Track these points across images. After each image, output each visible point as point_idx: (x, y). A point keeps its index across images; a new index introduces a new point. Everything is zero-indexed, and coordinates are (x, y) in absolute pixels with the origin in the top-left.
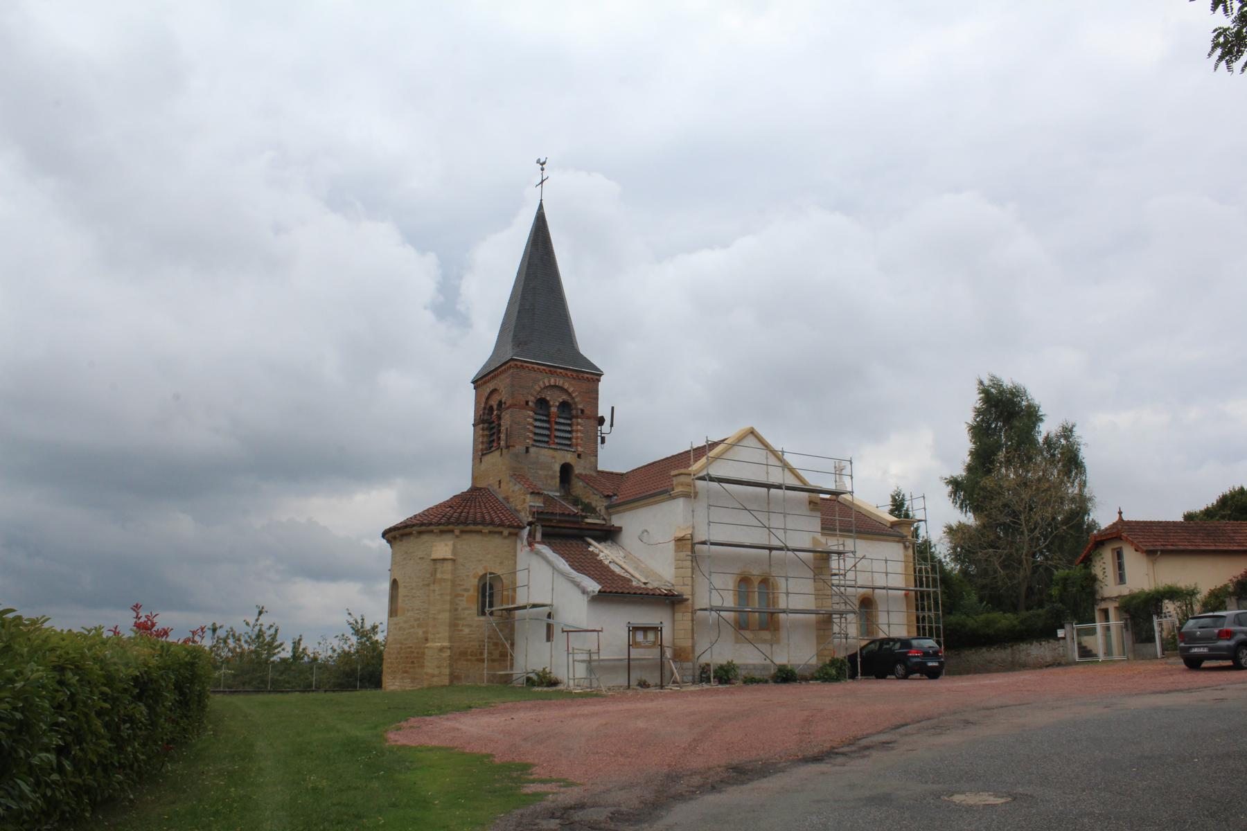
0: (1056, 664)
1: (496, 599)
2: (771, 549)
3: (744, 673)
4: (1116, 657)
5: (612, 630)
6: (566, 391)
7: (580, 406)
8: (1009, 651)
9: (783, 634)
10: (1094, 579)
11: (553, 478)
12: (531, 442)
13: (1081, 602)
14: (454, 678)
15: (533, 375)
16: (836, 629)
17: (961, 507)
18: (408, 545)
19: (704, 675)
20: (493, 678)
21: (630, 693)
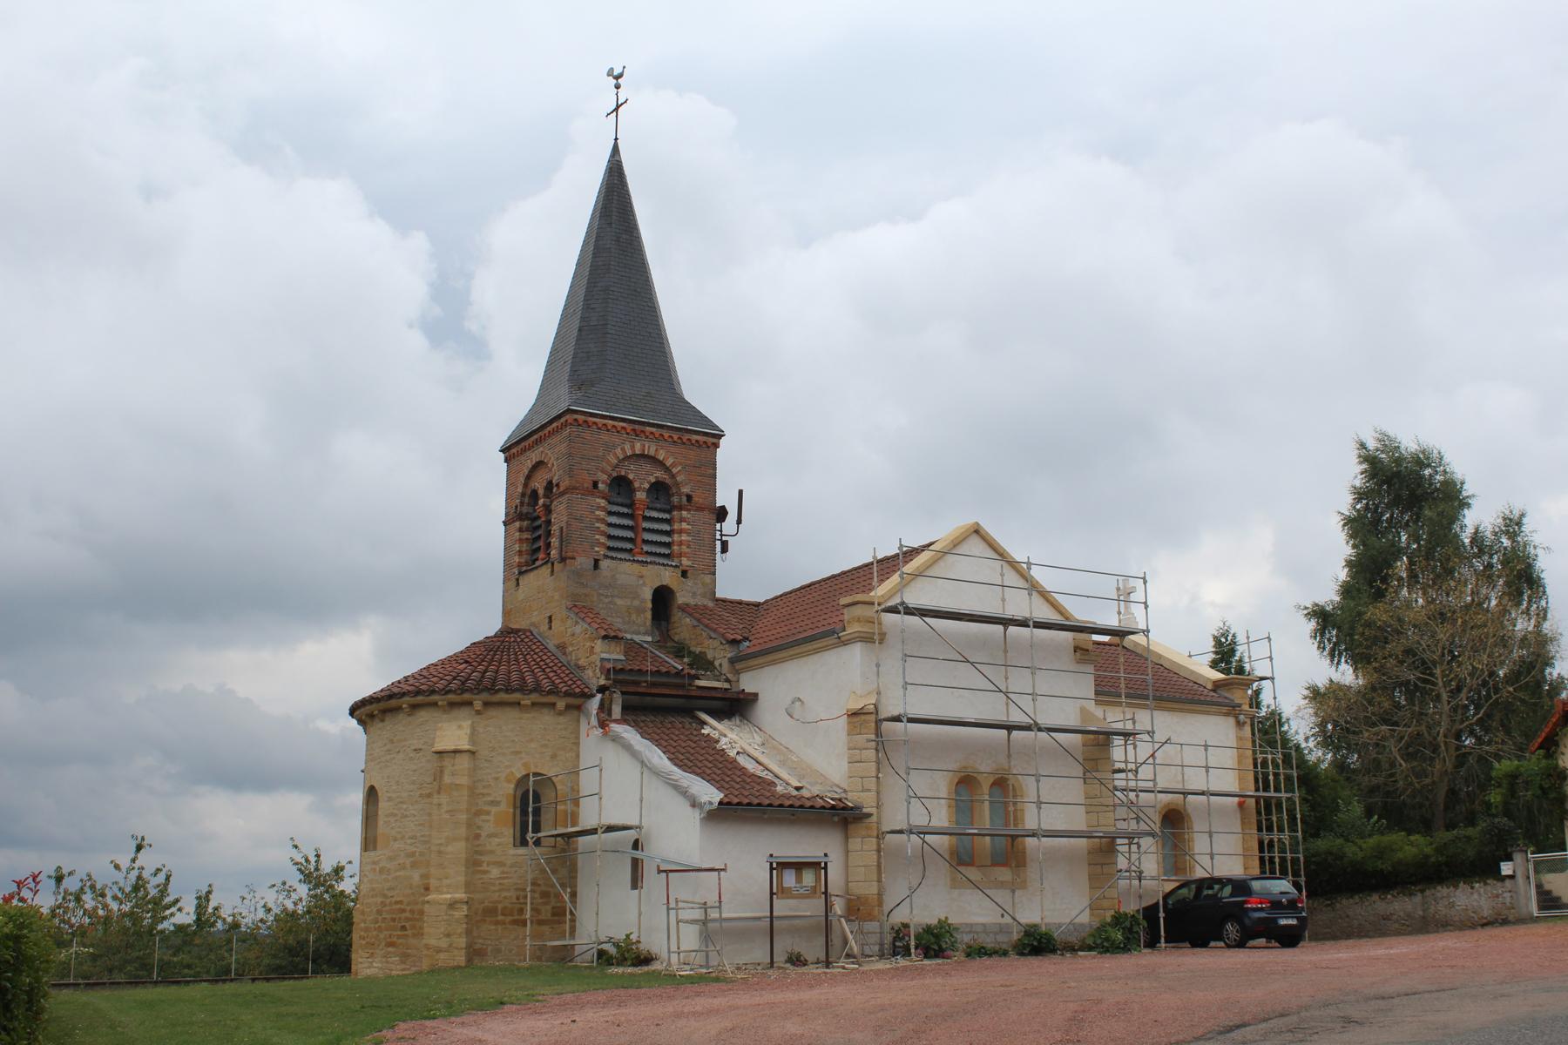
1: (547, 818)
2: (1010, 728)
3: (967, 938)
5: (744, 865)
6: (661, 464)
7: (686, 490)
8: (1418, 898)
9: (1032, 872)
11: (640, 611)
12: (603, 551)
14: (474, 953)
15: (605, 437)
16: (1122, 862)
17: (1332, 656)
18: (404, 728)
19: (898, 944)
20: (540, 953)
21: (773, 974)
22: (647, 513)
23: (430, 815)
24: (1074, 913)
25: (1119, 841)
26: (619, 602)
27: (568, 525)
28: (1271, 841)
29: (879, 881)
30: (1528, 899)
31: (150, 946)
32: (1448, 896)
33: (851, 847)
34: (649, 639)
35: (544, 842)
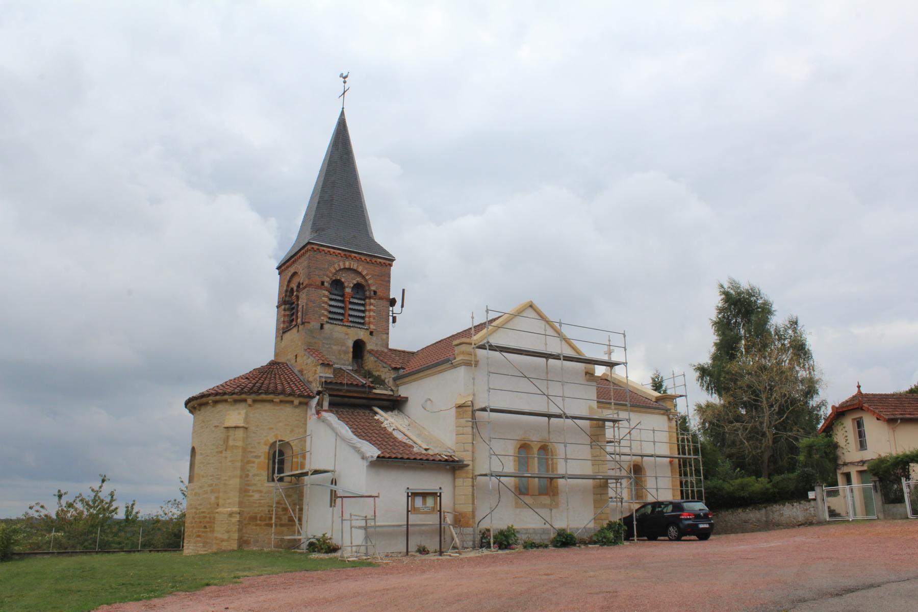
0: (808, 523)
1: (287, 466)
2: (549, 416)
3: (524, 537)
4: (859, 517)
5: (391, 493)
6: (360, 274)
7: (373, 288)
8: (763, 511)
9: (562, 499)
10: (836, 446)
11: (346, 352)
12: (326, 319)
13: (826, 468)
14: (243, 542)
15: (329, 258)
16: (611, 493)
17: (707, 389)
18: (207, 413)
19: (484, 541)
21: (406, 560)
22: (352, 300)
23: (221, 463)
24: (586, 523)
25: (609, 481)
26: (334, 347)
27: (307, 304)
28: (686, 482)
29: (473, 504)
30: (824, 511)
31: (95, 532)
32: (780, 510)
33: (457, 484)
34: (351, 368)
35: (287, 479)
